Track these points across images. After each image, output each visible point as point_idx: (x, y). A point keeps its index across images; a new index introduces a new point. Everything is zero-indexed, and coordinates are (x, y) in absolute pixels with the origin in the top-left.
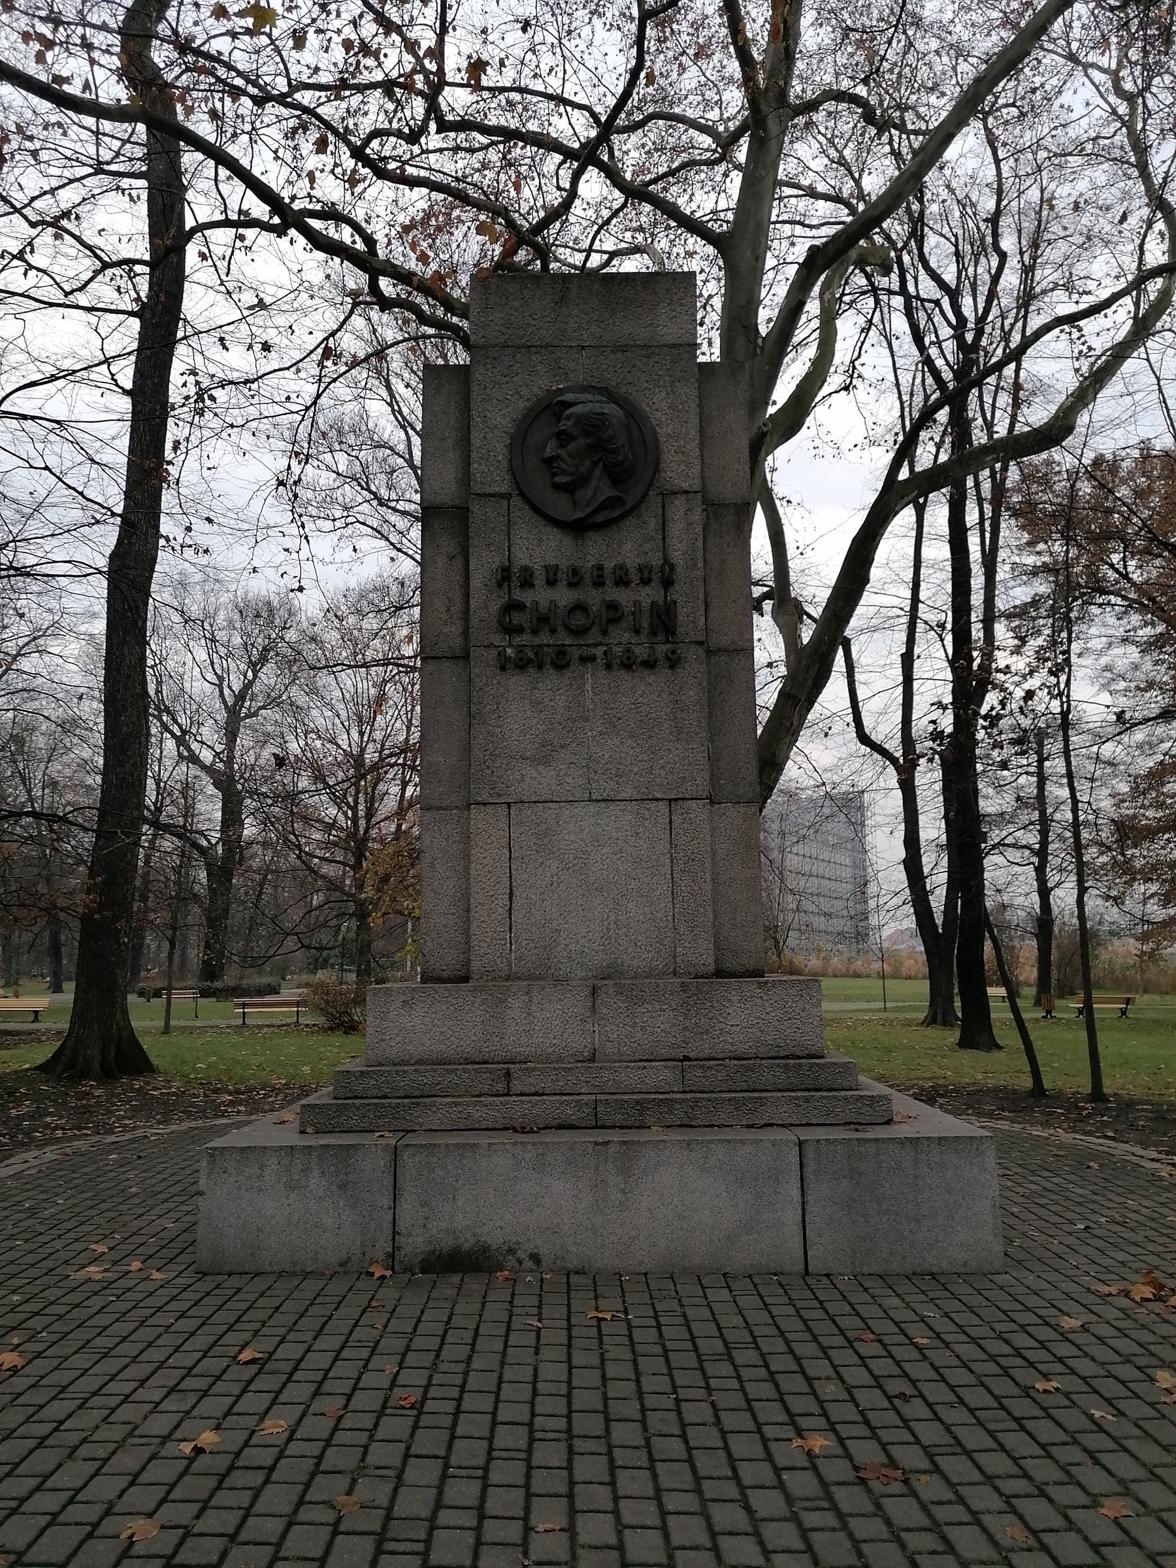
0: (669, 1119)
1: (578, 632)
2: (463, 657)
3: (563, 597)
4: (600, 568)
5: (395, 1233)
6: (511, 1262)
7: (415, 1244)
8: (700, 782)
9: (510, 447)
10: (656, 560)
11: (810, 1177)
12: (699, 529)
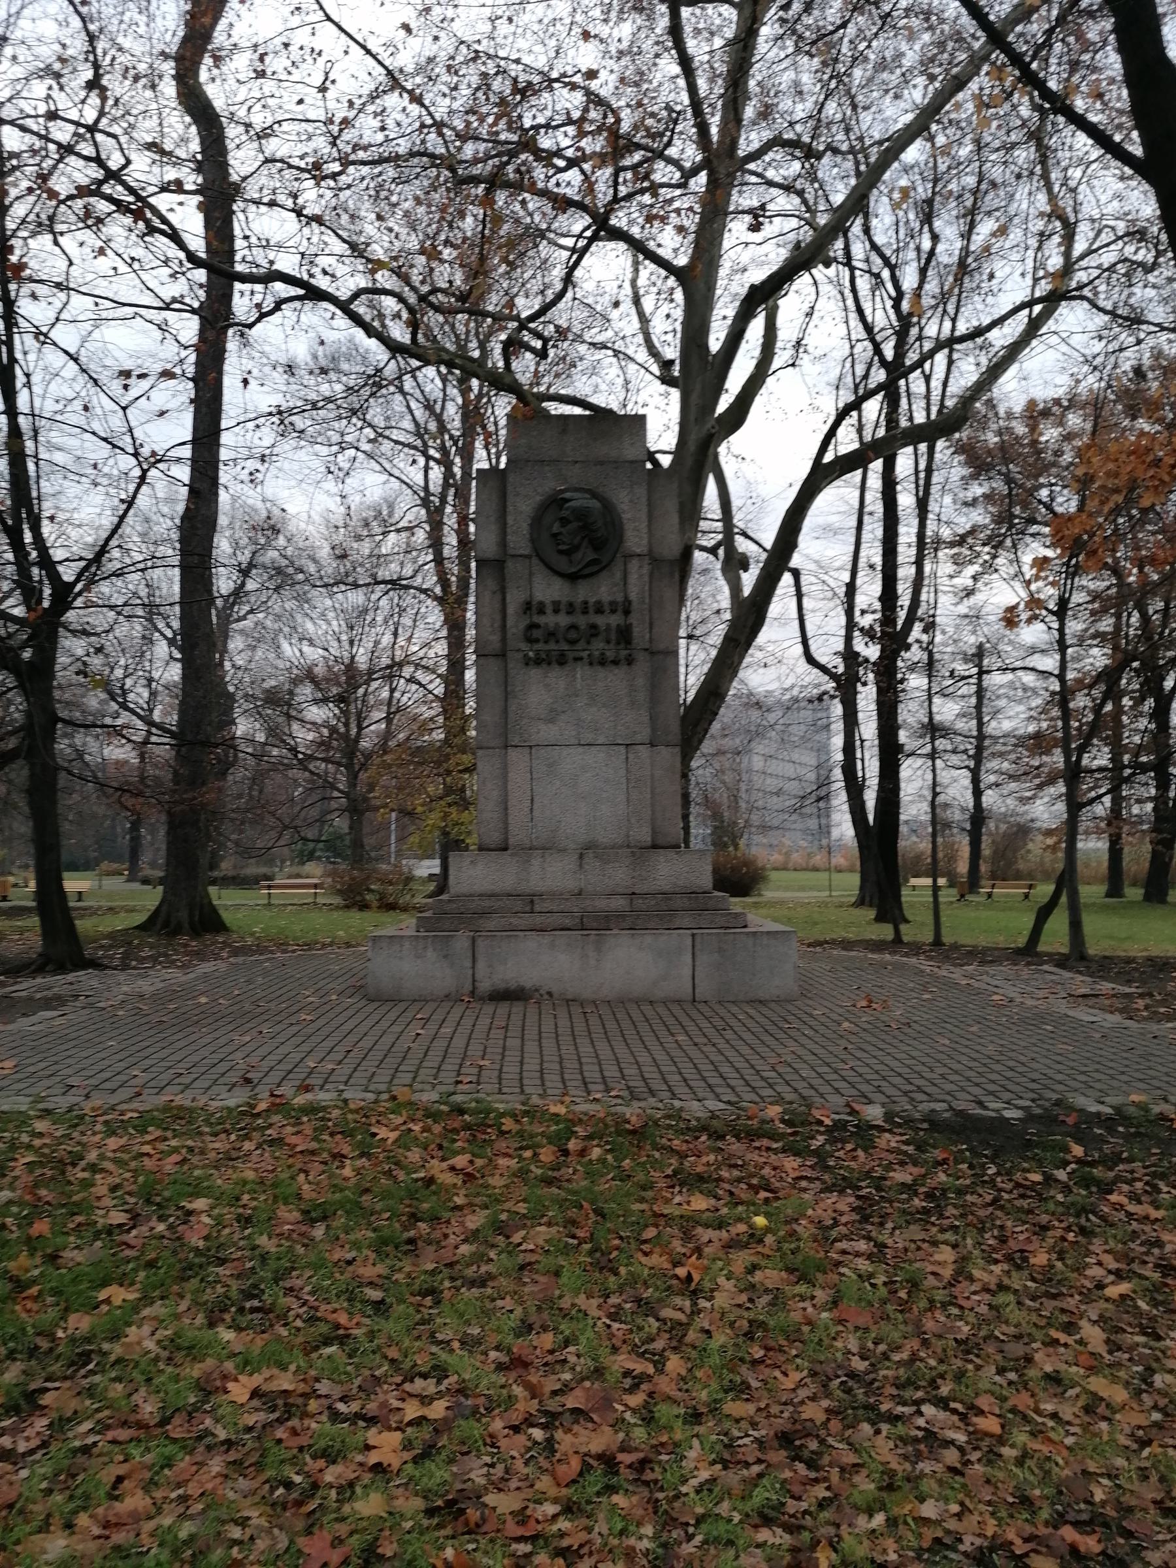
0: (625, 925)
1: (573, 642)
2: (502, 655)
3: (563, 620)
4: (586, 603)
5: (474, 981)
6: (537, 995)
7: (485, 986)
8: (644, 734)
9: (531, 525)
10: (620, 598)
11: (698, 953)
12: (646, 579)
